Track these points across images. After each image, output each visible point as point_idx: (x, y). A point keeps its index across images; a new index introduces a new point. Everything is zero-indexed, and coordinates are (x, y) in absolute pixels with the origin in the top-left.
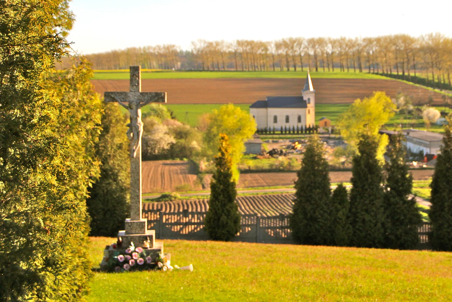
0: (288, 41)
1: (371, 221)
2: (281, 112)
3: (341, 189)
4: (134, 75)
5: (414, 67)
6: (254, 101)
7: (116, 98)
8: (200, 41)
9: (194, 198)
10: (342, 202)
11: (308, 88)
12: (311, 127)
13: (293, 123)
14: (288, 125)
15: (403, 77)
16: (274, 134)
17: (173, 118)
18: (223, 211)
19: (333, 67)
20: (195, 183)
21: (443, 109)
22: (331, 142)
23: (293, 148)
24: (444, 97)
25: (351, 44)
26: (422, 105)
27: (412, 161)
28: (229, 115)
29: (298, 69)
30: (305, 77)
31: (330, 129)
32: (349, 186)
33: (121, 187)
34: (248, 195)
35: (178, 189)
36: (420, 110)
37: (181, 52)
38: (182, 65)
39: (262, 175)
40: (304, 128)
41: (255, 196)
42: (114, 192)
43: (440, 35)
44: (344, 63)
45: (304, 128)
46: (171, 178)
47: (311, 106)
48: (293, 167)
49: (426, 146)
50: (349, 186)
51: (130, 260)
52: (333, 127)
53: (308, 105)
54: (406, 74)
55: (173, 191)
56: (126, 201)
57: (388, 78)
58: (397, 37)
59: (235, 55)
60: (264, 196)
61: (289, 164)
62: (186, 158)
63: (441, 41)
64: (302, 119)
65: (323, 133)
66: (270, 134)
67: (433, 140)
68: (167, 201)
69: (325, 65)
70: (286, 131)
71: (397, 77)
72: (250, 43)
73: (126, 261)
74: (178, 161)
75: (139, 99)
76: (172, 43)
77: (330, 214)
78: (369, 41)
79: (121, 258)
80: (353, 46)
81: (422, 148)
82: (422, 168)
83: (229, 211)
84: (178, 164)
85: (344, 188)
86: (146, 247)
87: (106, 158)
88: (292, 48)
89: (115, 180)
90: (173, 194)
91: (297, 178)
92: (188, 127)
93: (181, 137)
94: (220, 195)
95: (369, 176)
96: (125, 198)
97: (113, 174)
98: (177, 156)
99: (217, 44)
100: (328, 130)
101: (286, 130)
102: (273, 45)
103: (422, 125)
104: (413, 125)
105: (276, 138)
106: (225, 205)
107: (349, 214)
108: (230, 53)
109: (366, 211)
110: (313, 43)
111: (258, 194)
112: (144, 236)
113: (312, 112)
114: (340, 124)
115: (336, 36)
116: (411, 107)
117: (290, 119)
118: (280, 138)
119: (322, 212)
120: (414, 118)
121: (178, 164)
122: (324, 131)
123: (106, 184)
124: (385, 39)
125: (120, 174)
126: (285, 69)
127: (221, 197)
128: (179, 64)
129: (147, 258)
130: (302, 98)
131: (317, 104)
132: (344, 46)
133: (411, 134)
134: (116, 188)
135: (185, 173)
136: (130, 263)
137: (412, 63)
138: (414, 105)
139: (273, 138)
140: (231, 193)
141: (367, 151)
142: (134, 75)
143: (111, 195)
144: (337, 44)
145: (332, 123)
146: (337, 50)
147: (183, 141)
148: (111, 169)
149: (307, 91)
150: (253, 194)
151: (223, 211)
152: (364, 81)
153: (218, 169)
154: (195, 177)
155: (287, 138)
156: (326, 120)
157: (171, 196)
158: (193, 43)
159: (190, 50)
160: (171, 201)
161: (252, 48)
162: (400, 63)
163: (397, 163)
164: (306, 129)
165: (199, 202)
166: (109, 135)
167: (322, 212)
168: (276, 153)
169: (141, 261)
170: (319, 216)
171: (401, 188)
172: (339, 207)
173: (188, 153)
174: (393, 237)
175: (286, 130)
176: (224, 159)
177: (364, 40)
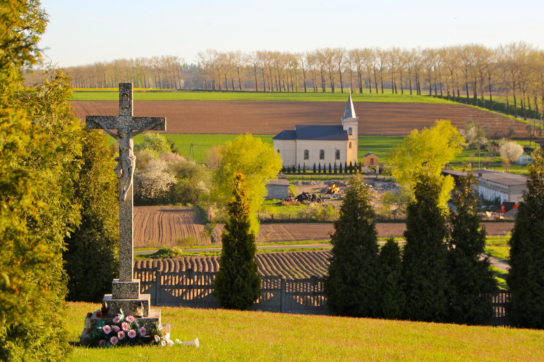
1: (430, 288)
3: (391, 246)
4: (124, 94)
5: (490, 88)
7: (101, 123)
9: (201, 255)
10: (393, 262)
12: (353, 165)
13: (330, 160)
14: (322, 163)
15: (474, 101)
16: (304, 173)
18: (238, 271)
20: (202, 235)
21: (527, 143)
22: (379, 184)
23: (330, 192)
24: (529, 127)
25: (407, 57)
31: (377, 169)
32: (401, 242)
34: (270, 252)
35: (180, 243)
36: (497, 145)
39: (288, 226)
40: (343, 166)
41: (280, 253)
43: (525, 46)
44: (398, 82)
45: (343, 166)
46: (171, 228)
47: (353, 138)
48: (329, 216)
49: (503, 191)
50: (401, 242)
53: (350, 137)
54: (479, 97)
56: (112, 257)
58: (467, 49)
60: (290, 253)
61: (324, 213)
62: (191, 203)
63: (527, 54)
64: (342, 155)
65: (368, 174)
66: (299, 173)
67: (513, 183)
68: (166, 257)
70: (320, 171)
71: (467, 101)
72: (275, 56)
74: (180, 206)
76: (174, 55)
78: (431, 54)
79: (107, 329)
80: (410, 60)
81: (498, 194)
82: (498, 221)
83: (245, 271)
84: (181, 211)
86: (139, 315)
87: (88, 202)
88: (329, 62)
89: (99, 230)
91: (334, 231)
92: (193, 163)
93: (185, 176)
98: (179, 201)
99: (232, 56)
100: (375, 170)
103: (499, 164)
104: (486, 164)
105: (307, 179)
106: (240, 264)
107: (402, 278)
108: (248, 68)
109: (424, 274)
110: (356, 55)
111: (283, 251)
112: (136, 301)
113: (355, 146)
115: (386, 46)
116: (485, 141)
118: (313, 179)
119: (366, 275)
121: (181, 211)
122: (369, 170)
124: (452, 50)
126: (320, 89)
129: (140, 330)
130: (342, 127)
131: (361, 136)
133: (484, 176)
135: (189, 222)
136: (119, 336)
137: (487, 83)
138: (488, 137)
139: (303, 179)
142: (124, 94)
144: (388, 57)
145: (381, 161)
147: (186, 181)
148: (95, 216)
149: (349, 119)
150: (277, 250)
151: (238, 271)
154: (202, 228)
155: (322, 179)
157: (171, 252)
160: (171, 258)
161: (277, 62)
164: (346, 168)
165: (207, 259)
166: (92, 172)
167: (366, 275)
168: (306, 198)
169: (132, 333)
170: (363, 280)
172: (388, 268)
173: (194, 196)
176: (240, 205)
177: (424, 52)
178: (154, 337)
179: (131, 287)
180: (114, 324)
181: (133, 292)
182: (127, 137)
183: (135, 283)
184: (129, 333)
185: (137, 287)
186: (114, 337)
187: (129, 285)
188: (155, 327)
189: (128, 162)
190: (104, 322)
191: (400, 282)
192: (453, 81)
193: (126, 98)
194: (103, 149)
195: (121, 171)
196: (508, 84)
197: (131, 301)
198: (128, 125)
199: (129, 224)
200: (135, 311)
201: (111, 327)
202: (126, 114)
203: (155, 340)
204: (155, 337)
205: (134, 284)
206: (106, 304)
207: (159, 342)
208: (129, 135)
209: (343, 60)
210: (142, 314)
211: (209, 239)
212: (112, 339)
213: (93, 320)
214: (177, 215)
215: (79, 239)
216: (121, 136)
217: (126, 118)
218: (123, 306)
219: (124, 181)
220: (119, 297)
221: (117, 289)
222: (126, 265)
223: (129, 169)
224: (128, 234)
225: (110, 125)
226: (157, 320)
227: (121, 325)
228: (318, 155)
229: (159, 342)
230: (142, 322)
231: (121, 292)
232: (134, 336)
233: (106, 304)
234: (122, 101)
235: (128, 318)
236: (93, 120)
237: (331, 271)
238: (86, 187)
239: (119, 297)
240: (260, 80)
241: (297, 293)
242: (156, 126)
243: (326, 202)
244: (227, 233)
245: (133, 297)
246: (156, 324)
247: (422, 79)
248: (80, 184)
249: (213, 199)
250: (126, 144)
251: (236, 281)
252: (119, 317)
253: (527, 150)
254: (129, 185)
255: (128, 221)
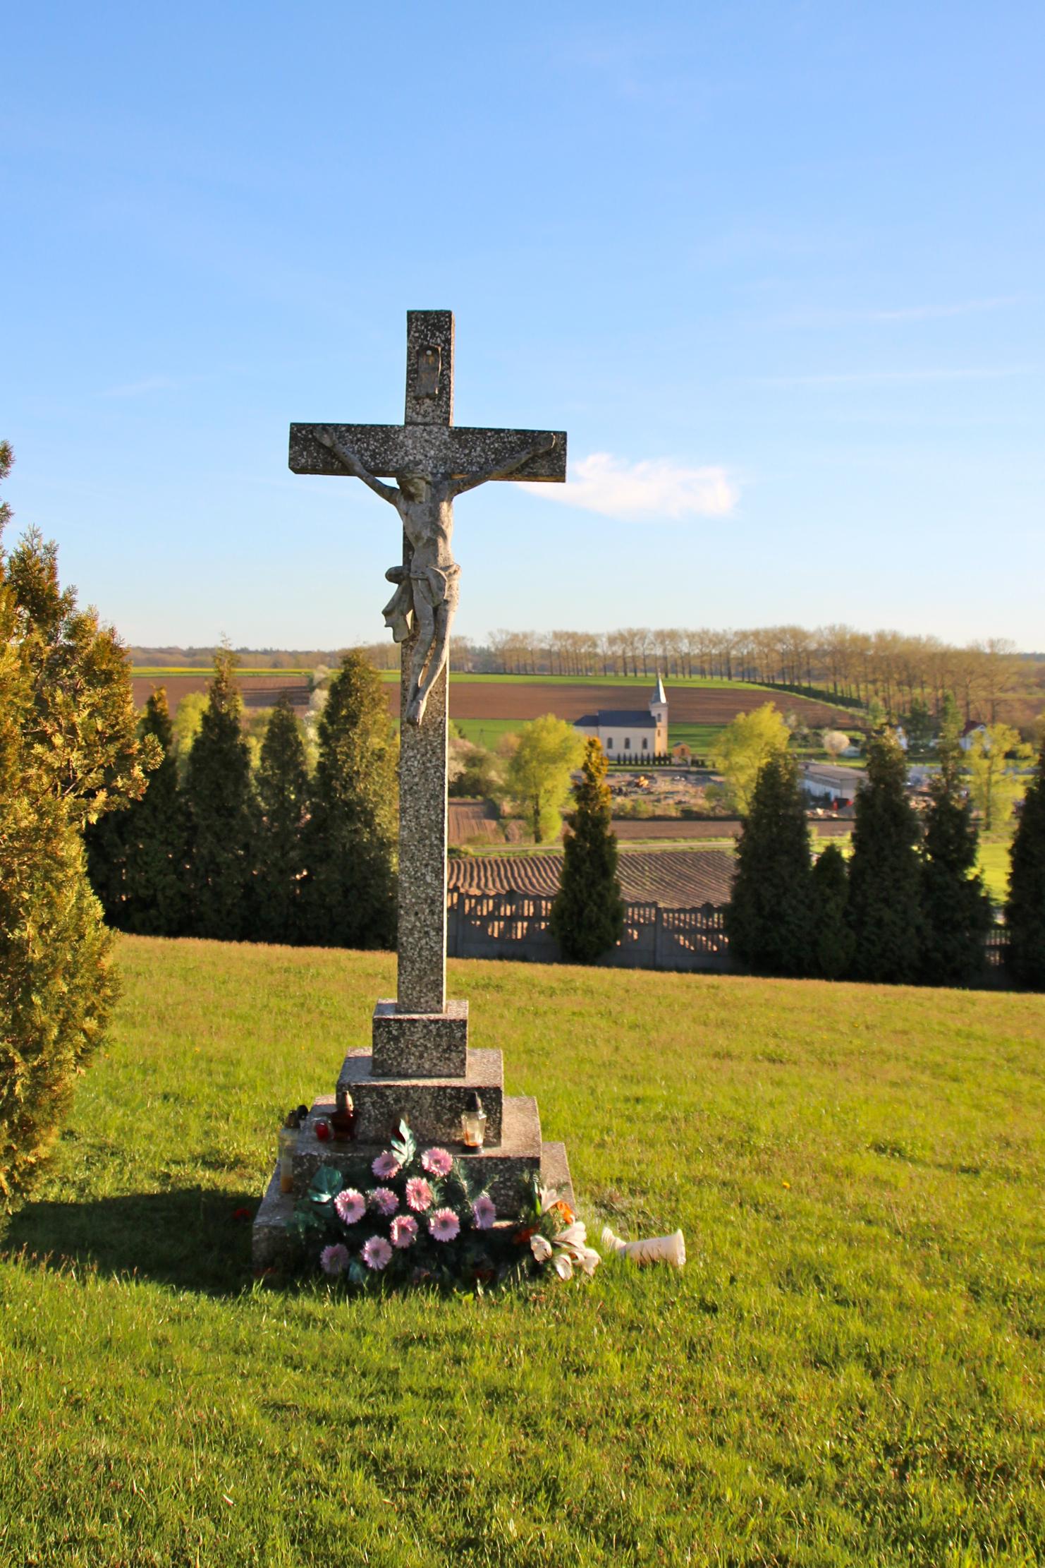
0: (626, 634)
1: (894, 923)
2: (618, 734)
3: (831, 854)
4: (424, 349)
5: (809, 674)
6: (579, 717)
7: (341, 449)
8: (501, 631)
9: (494, 856)
10: (834, 882)
11: (658, 699)
13: (636, 749)
14: (628, 753)
15: (791, 688)
17: (462, 737)
18: (590, 896)
19: (690, 673)
20: (496, 832)
21: (852, 733)
22: (692, 777)
23: (638, 785)
24: (852, 717)
25: (717, 640)
26: (820, 727)
27: (814, 807)
28: (549, 732)
29: (640, 675)
30: (654, 685)
31: (689, 759)
32: (847, 853)
33: (380, 840)
35: (470, 841)
36: (818, 735)
37: (473, 649)
38: (474, 667)
42: (367, 848)
44: (706, 667)
47: (662, 726)
49: (834, 785)
50: (847, 853)
51: (391, 1218)
52: (693, 756)
54: (796, 684)
55: (461, 844)
56: (389, 868)
57: (770, 689)
58: (783, 631)
59: (548, 654)
61: (634, 809)
63: (848, 637)
64: (649, 744)
65: (679, 765)
69: (679, 669)
71: (783, 687)
72: (572, 636)
73: (376, 1222)
74: (469, 799)
75: (445, 460)
76: (462, 634)
77: (810, 908)
78: (744, 636)
79: (350, 1205)
80: (720, 642)
82: (831, 819)
83: (601, 896)
84: (469, 804)
85: (839, 855)
86: (470, 1143)
87: (351, 779)
88: (632, 643)
89: (369, 823)
90: (464, 848)
91: (740, 832)
92: (483, 750)
93: (474, 765)
94: (584, 862)
95: (892, 829)
96: (389, 862)
97: (364, 811)
98: (468, 793)
99: (525, 636)
101: (625, 759)
102: (604, 640)
103: (824, 756)
104: (810, 756)
106: (593, 884)
107: (851, 909)
108: (542, 650)
109: (886, 901)
110: (662, 636)
112: (458, 1089)
114: (715, 751)
115: (694, 626)
116: (806, 731)
117: (632, 744)
119: (794, 902)
120: (811, 746)
121: (469, 804)
122: (680, 762)
123: (350, 832)
124: (766, 632)
125: (377, 812)
126: (622, 674)
127: (587, 867)
128: (470, 665)
129: (474, 1206)
130: (649, 713)
131: (672, 723)
132: (707, 642)
133: (811, 768)
134: (370, 842)
135: (479, 817)
136: (395, 1235)
137: (805, 668)
138: (809, 727)
140: (607, 858)
141: (888, 779)
142: (424, 349)
143: (360, 856)
144: (697, 638)
146: (696, 651)
147: (476, 770)
148: (361, 802)
151: (590, 896)
152: (735, 692)
153: (581, 808)
154: (494, 824)
156: (684, 746)
158: (491, 634)
159: (485, 646)
161: (574, 644)
162: (788, 667)
163: (948, 804)
164: (655, 759)
166: (358, 731)
167: (794, 902)
169: (445, 1223)
170: (790, 911)
171: (955, 856)
172: (828, 891)
173: (484, 788)
174: (937, 956)
175: (625, 759)
176: (594, 788)
177: (736, 634)
178: (529, 1243)
179: (439, 1035)
180: (377, 1182)
181: (444, 1051)
182: (433, 496)
183: (454, 1021)
184: (432, 1221)
185: (459, 1035)
186: (376, 1238)
187: (432, 1027)
188: (528, 1197)
189: (433, 582)
190: (338, 1175)
191: (846, 914)
192: (768, 665)
193: (431, 359)
194: (376, 695)
195: (409, 616)
196: (828, 669)
197: (440, 1088)
198: (435, 458)
199: (435, 807)
200: (454, 1123)
201: (366, 1196)
202: (428, 419)
203: (531, 1253)
204: (534, 1245)
205: (449, 1024)
206: (349, 1100)
207: (549, 1260)
208: (438, 491)
209: (647, 641)
210: (479, 1139)
211: (503, 838)
212: (368, 1246)
213: (302, 1157)
214: (464, 809)
215: (336, 839)
216: (412, 490)
217: (430, 433)
218: (408, 1106)
219: (418, 652)
220: (395, 1070)
221: (389, 1040)
222: (420, 956)
223: (436, 610)
224: (431, 845)
225: (373, 457)
226: (534, 1163)
227: (404, 1188)
228: (623, 743)
229: (549, 1260)
230: (480, 1171)
231: (402, 1051)
232: (453, 1232)
233: (349, 1100)
234: (416, 371)
235: (431, 1155)
236: (314, 439)
237: (737, 895)
238: (347, 755)
239: (395, 1070)
240: (556, 663)
241: (679, 930)
242: (533, 460)
243: (634, 797)
244: (573, 834)
245: (446, 1071)
246: (531, 1184)
247: (733, 664)
248: (338, 750)
249: (505, 791)
250: (427, 519)
251: (586, 912)
252: (395, 1154)
253: (853, 741)
254: (436, 667)
255: (432, 796)
